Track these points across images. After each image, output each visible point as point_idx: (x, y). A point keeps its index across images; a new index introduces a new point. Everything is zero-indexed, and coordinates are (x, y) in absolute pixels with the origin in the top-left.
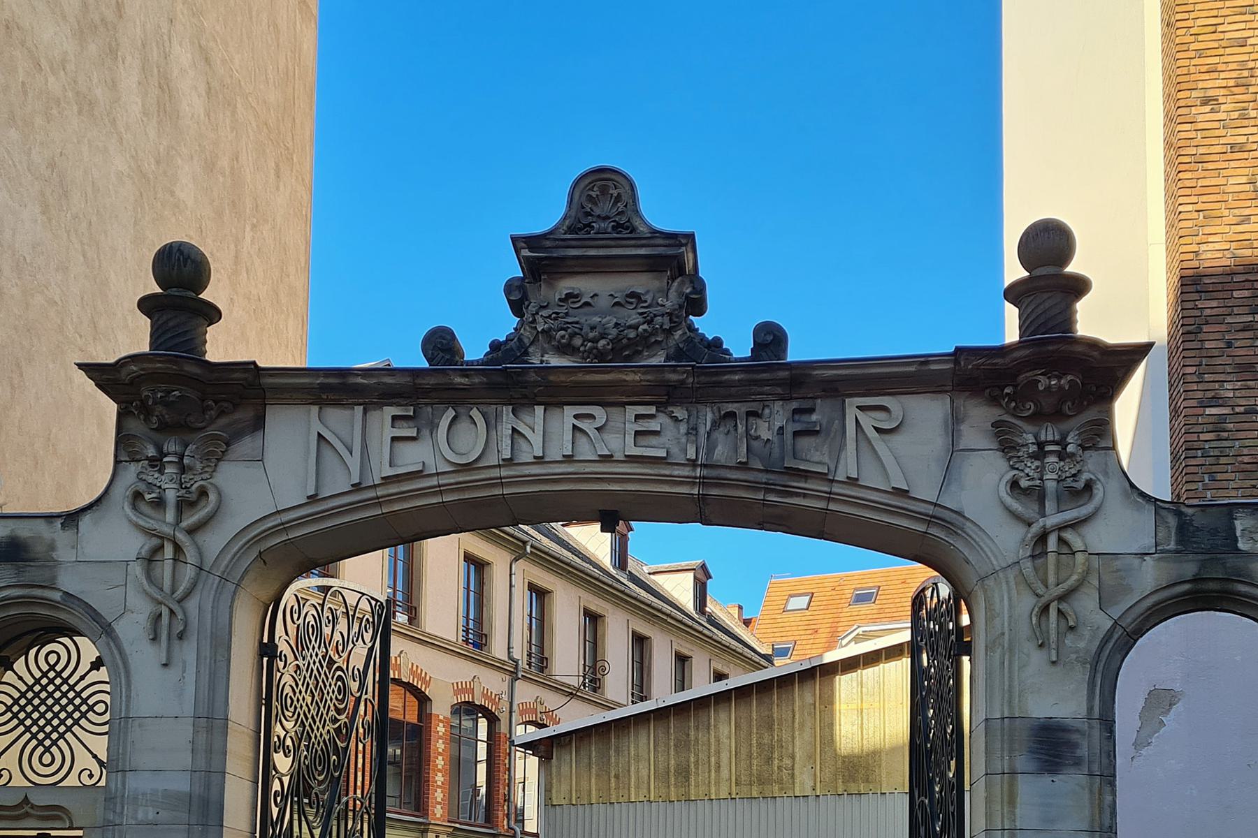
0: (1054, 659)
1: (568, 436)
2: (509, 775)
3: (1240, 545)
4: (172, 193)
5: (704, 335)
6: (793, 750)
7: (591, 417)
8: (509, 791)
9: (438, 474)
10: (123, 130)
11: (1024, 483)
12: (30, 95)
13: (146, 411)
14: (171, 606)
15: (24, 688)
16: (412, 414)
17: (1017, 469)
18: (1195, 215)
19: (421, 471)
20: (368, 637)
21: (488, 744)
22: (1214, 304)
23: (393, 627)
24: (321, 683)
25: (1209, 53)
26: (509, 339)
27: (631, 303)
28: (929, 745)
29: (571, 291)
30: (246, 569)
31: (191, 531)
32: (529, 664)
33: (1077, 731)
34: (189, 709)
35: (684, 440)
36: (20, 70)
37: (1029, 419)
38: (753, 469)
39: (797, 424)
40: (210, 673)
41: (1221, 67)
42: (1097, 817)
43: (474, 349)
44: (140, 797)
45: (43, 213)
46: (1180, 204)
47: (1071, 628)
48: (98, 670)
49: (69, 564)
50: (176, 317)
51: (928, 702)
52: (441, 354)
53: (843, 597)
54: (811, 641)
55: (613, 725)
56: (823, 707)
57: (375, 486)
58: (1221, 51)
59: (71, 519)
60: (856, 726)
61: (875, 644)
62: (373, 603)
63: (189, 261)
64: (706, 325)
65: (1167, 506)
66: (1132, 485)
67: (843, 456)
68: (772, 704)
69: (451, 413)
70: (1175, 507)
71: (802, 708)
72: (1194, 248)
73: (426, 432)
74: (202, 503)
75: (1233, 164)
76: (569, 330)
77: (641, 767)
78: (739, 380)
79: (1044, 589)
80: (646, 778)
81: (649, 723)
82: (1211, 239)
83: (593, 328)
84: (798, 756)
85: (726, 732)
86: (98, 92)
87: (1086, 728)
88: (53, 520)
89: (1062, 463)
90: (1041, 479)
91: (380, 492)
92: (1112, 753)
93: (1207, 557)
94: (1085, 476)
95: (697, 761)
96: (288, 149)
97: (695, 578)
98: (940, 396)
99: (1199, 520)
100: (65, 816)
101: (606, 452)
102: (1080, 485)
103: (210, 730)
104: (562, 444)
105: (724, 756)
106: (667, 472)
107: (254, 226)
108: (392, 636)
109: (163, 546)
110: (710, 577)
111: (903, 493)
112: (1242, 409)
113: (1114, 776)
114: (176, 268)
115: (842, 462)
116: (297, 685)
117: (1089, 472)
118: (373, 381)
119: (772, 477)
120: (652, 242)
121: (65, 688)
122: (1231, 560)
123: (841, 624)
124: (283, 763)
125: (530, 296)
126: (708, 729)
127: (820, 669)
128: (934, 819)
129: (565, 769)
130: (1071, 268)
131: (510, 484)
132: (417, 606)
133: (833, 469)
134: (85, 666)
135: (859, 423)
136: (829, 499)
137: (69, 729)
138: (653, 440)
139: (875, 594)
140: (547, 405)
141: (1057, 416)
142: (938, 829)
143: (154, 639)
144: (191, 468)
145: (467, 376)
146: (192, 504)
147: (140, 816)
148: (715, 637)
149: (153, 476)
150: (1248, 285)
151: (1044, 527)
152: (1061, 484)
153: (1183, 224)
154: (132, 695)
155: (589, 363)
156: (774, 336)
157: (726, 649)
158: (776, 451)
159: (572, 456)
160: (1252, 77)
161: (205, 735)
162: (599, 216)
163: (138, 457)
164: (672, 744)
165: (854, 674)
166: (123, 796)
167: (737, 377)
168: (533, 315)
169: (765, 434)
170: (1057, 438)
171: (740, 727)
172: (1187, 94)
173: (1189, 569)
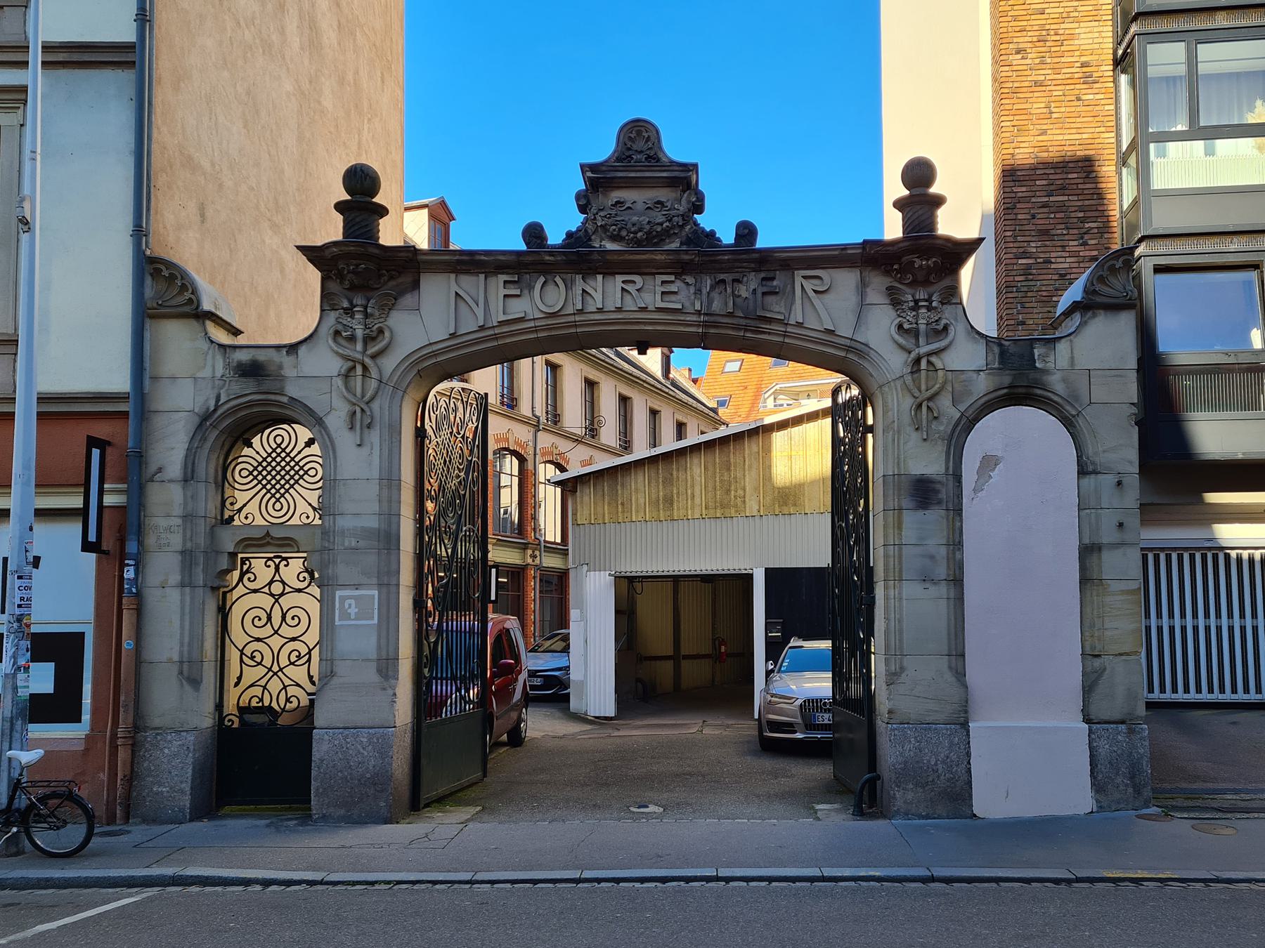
0: (925, 437)
1: (619, 295)
2: (535, 500)
3: (1037, 365)
4: (319, 103)
5: (704, 228)
6: (744, 484)
7: (634, 282)
8: (535, 512)
9: (534, 319)
10: (289, 63)
11: (906, 326)
12: (235, 45)
13: (341, 277)
14: (362, 406)
16: (516, 279)
17: (902, 317)
18: (1012, 129)
19: (524, 317)
20: (474, 418)
21: (519, 478)
22: (1024, 189)
23: (489, 408)
24: (450, 453)
25: (1021, 18)
26: (579, 230)
27: (658, 208)
28: (845, 489)
29: (618, 199)
31: (373, 357)
32: (547, 420)
33: (939, 482)
34: (376, 474)
35: (693, 297)
36: (229, 28)
37: (909, 285)
38: (737, 316)
39: (765, 288)
41: (1028, 28)
42: (951, 536)
43: (555, 237)
45: (245, 127)
46: (1002, 121)
47: (936, 418)
48: (310, 447)
51: (844, 461)
52: (535, 240)
54: (742, 395)
56: (764, 454)
57: (494, 327)
58: (1028, 17)
59: (293, 348)
60: (787, 468)
62: (477, 395)
63: (368, 178)
64: (705, 221)
65: (993, 340)
66: (972, 327)
67: (793, 308)
68: (729, 452)
69: (542, 279)
70: (998, 341)
71: (750, 455)
72: (1011, 151)
73: (526, 292)
74: (380, 338)
75: (1036, 94)
76: (619, 226)
77: (639, 497)
78: (728, 259)
79: (919, 394)
80: (643, 505)
81: (645, 466)
82: (1022, 145)
83: (634, 225)
84: (747, 488)
85: (698, 471)
86: (274, 37)
87: (945, 481)
88: (281, 349)
89: (929, 313)
90: (916, 323)
92: (960, 496)
93: (1018, 372)
94: (943, 322)
95: (679, 492)
96: (389, 61)
97: (662, 353)
99: (1013, 349)
100: (295, 545)
101: (644, 306)
102: (940, 327)
103: (390, 487)
104: (614, 300)
106: (682, 318)
107: (369, 120)
108: (489, 414)
109: (355, 367)
112: (1042, 260)
113: (962, 510)
115: (793, 312)
116: (437, 455)
117: (946, 319)
119: (748, 321)
120: (671, 168)
121: (288, 459)
122: (1032, 375)
123: (763, 382)
124: (430, 505)
125: (592, 202)
126: (686, 470)
128: (849, 537)
129: (586, 499)
130: (934, 190)
132: (467, 378)
133: (787, 316)
134: (301, 445)
135: (805, 289)
136: (785, 336)
137: (292, 486)
138: (673, 298)
140: (605, 274)
141: (926, 283)
142: (852, 543)
143: (351, 428)
144: (372, 315)
145: (553, 256)
146: (373, 339)
147: (346, 544)
148: (677, 396)
149: (347, 320)
150: (1045, 177)
152: (929, 326)
153: (1003, 135)
155: (632, 247)
156: (750, 230)
157: (685, 405)
158: (751, 306)
159: (621, 308)
160: (1048, 35)
162: (636, 151)
163: (337, 307)
165: (786, 431)
166: (334, 531)
167: (726, 257)
168: (594, 215)
169: (744, 294)
170: (926, 297)
172: (1006, 46)
173: (1007, 380)
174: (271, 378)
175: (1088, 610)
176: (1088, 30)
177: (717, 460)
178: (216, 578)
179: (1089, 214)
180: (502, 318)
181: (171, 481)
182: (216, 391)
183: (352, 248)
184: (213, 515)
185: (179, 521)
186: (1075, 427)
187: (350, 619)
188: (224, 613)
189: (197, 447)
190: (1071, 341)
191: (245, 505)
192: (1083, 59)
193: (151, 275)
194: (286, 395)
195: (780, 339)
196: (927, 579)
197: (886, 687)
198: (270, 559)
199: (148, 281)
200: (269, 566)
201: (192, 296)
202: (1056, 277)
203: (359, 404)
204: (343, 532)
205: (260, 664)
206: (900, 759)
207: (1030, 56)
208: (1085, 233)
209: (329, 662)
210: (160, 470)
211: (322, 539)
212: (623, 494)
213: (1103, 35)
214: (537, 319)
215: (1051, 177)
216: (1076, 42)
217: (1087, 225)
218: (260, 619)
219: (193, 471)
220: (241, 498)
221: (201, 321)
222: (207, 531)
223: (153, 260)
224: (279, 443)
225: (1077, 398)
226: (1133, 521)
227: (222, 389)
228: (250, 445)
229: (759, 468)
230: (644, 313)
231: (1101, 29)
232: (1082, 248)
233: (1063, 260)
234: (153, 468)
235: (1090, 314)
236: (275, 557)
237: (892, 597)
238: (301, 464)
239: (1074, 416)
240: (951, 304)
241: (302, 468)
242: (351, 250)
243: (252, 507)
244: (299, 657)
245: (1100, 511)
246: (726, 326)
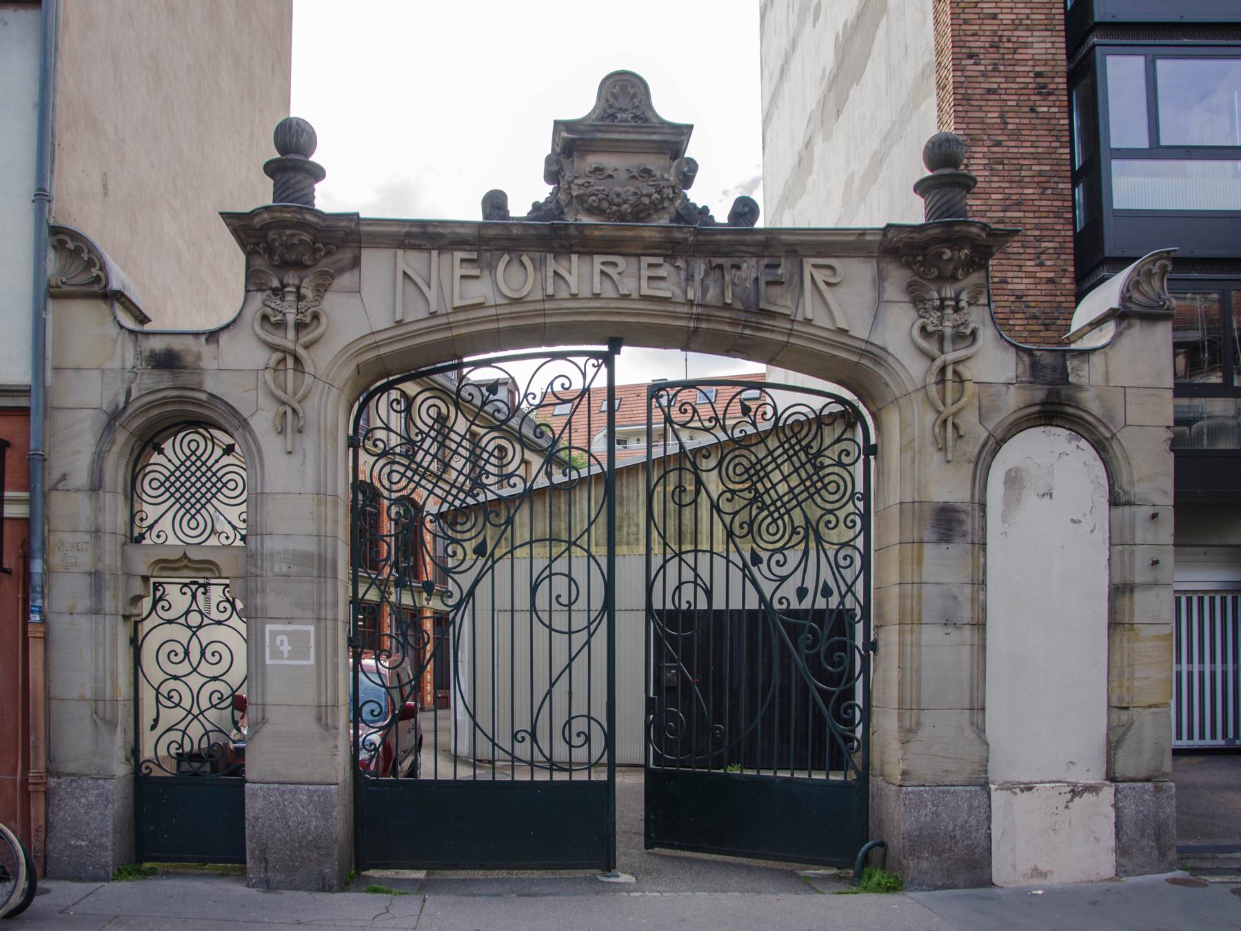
9: (496, 306)
15: (173, 469)
22: (979, 202)
26: (548, 201)
33: (964, 511)
35: (684, 285)
37: (932, 280)
41: (981, 33)
43: (519, 208)
57: (447, 314)
59: (212, 336)
64: (697, 195)
67: (801, 302)
69: (506, 258)
73: (486, 273)
91: (452, 319)
98: (869, 260)
111: (843, 332)
115: (801, 307)
131: (551, 315)
138: (661, 284)
140: (580, 253)
147: (277, 569)
149: (276, 303)
150: (1001, 191)
151: (945, 362)
163: (264, 288)
168: (569, 183)
175: (1117, 658)
176: (1040, 39)
179: (1045, 233)
180: (457, 303)
181: (77, 490)
182: (126, 386)
186: (1107, 452)
187: (282, 658)
188: (136, 645)
190: (1106, 354)
191: (156, 522)
192: (1037, 69)
193: (54, 247)
194: (205, 392)
195: (784, 339)
196: (949, 623)
197: (900, 745)
198: (185, 585)
199: (51, 254)
200: (185, 594)
201: (100, 273)
202: (1012, 299)
204: (272, 555)
205: (178, 705)
206: (915, 825)
207: (982, 62)
208: (1041, 253)
209: (260, 707)
210: (64, 477)
213: (1056, 45)
214: (500, 305)
215: (1007, 191)
216: (1029, 51)
217: (1044, 245)
218: (176, 655)
220: (151, 513)
223: (56, 231)
224: (193, 449)
225: (1112, 419)
226: (1168, 558)
227: (132, 382)
228: (161, 452)
230: (626, 302)
231: (1054, 39)
232: (1038, 269)
233: (1019, 280)
234: (56, 475)
235: (1125, 324)
236: (192, 583)
237: (909, 643)
239: (1107, 439)
240: (978, 305)
241: (219, 479)
244: (221, 699)
245: (1132, 547)
246: (720, 320)
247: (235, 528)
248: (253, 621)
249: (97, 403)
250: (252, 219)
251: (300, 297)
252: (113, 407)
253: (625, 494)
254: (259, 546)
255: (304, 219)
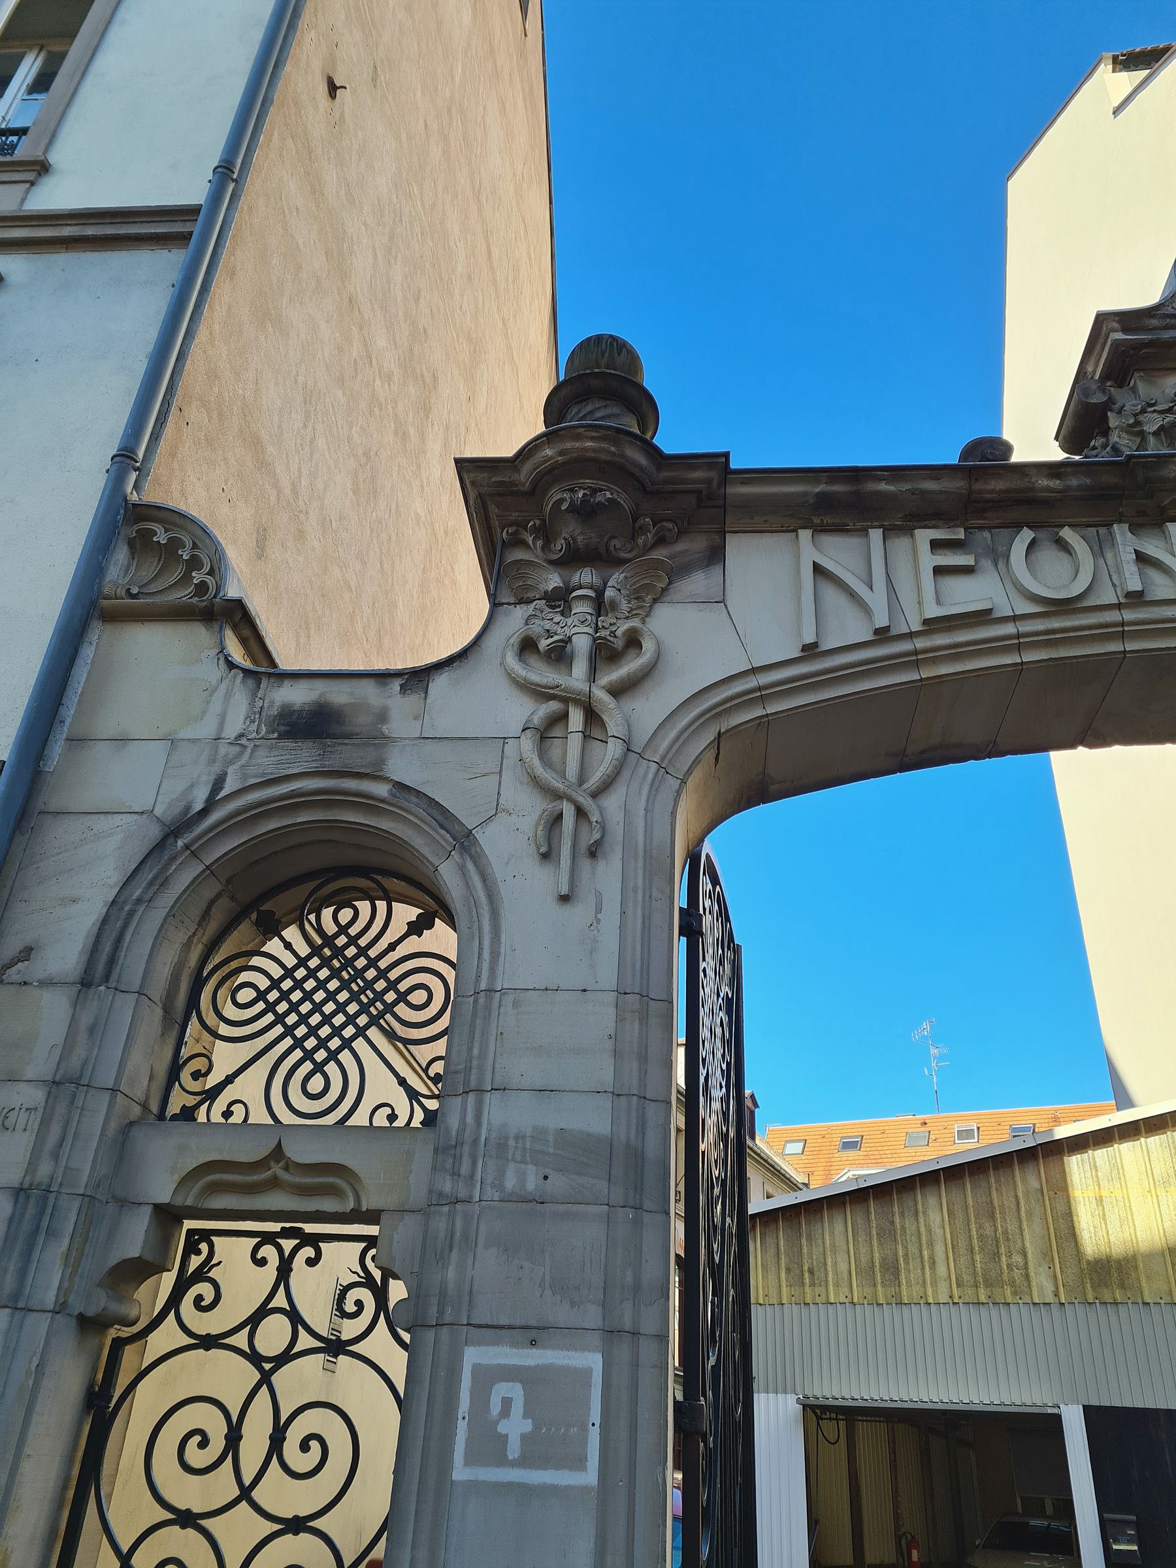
6: (1024, 1245)
14: (581, 799)
30: (697, 757)
34: (607, 976)
40: (644, 917)
44: (511, 1142)
49: (407, 742)
50: (605, 406)
53: (833, 1144)
55: (803, 1207)
57: (911, 635)
61: (1110, 1120)
63: (624, 350)
69: (1027, 535)
71: (1027, 1194)
77: (839, 1259)
80: (846, 1275)
85: (938, 1219)
91: (920, 643)
105: (939, 1249)
110: (758, 1107)
114: (607, 355)
118: (905, 487)
123: (833, 1168)
127: (1041, 1148)
139: (859, 1143)
147: (510, 1182)
154: (502, 950)
161: (637, 1026)
163: (531, 595)
164: (874, 1233)
166: (475, 1142)
171: (954, 1215)
174: (356, 741)
177: (970, 1201)
178: (100, 1285)
180: (933, 611)
181: (47, 983)
182: (216, 769)
183: (589, 444)
184: (139, 1094)
185: (36, 1096)
187: (501, 1460)
189: (139, 901)
191: (229, 1080)
193: (131, 543)
194: (385, 779)
198: (268, 1238)
199: (121, 554)
200: (262, 1262)
201: (209, 580)
203: (574, 795)
210: (27, 953)
211: (434, 1169)
212: (810, 1254)
218: (204, 1444)
219: (112, 961)
220: (226, 1058)
221: (216, 627)
222: (110, 1133)
229: (1046, 1218)
238: (393, 975)
242: (586, 449)
243: (249, 1087)
247: (412, 1094)
248: (430, 1335)
249: (144, 803)
250: (517, 469)
251: (600, 605)
252: (177, 810)
253: (996, 1202)
254: (470, 1119)
255: (622, 456)
